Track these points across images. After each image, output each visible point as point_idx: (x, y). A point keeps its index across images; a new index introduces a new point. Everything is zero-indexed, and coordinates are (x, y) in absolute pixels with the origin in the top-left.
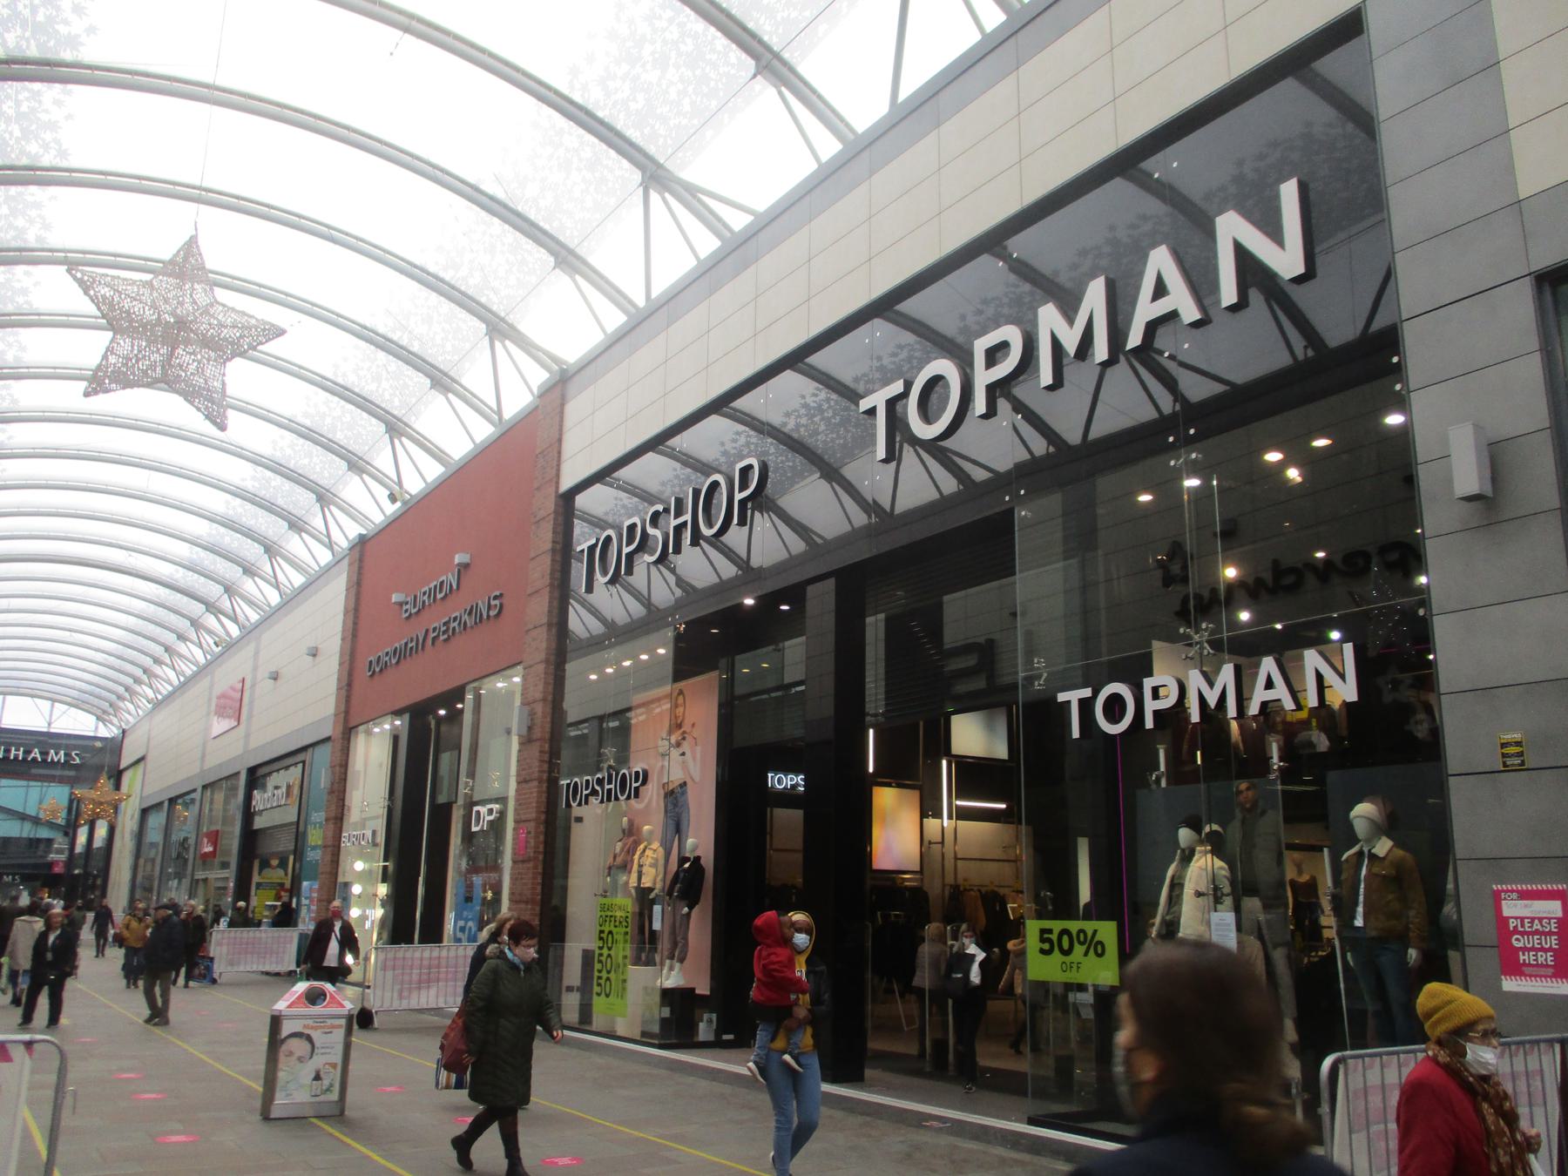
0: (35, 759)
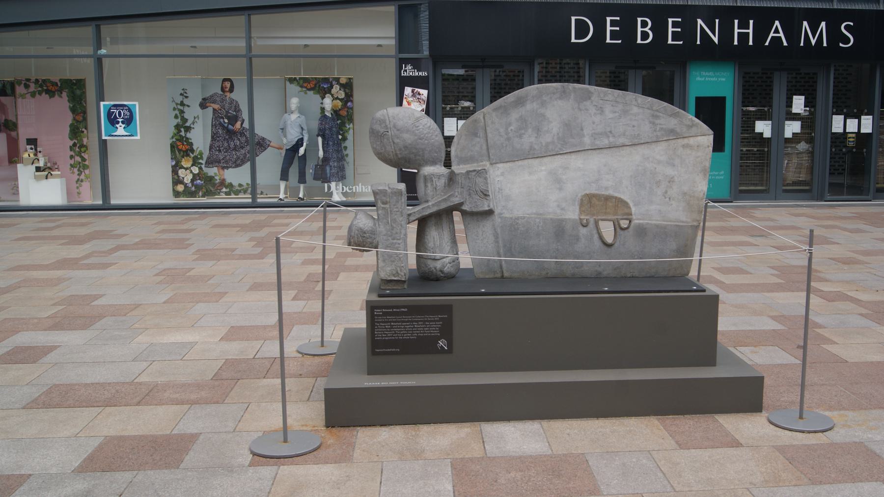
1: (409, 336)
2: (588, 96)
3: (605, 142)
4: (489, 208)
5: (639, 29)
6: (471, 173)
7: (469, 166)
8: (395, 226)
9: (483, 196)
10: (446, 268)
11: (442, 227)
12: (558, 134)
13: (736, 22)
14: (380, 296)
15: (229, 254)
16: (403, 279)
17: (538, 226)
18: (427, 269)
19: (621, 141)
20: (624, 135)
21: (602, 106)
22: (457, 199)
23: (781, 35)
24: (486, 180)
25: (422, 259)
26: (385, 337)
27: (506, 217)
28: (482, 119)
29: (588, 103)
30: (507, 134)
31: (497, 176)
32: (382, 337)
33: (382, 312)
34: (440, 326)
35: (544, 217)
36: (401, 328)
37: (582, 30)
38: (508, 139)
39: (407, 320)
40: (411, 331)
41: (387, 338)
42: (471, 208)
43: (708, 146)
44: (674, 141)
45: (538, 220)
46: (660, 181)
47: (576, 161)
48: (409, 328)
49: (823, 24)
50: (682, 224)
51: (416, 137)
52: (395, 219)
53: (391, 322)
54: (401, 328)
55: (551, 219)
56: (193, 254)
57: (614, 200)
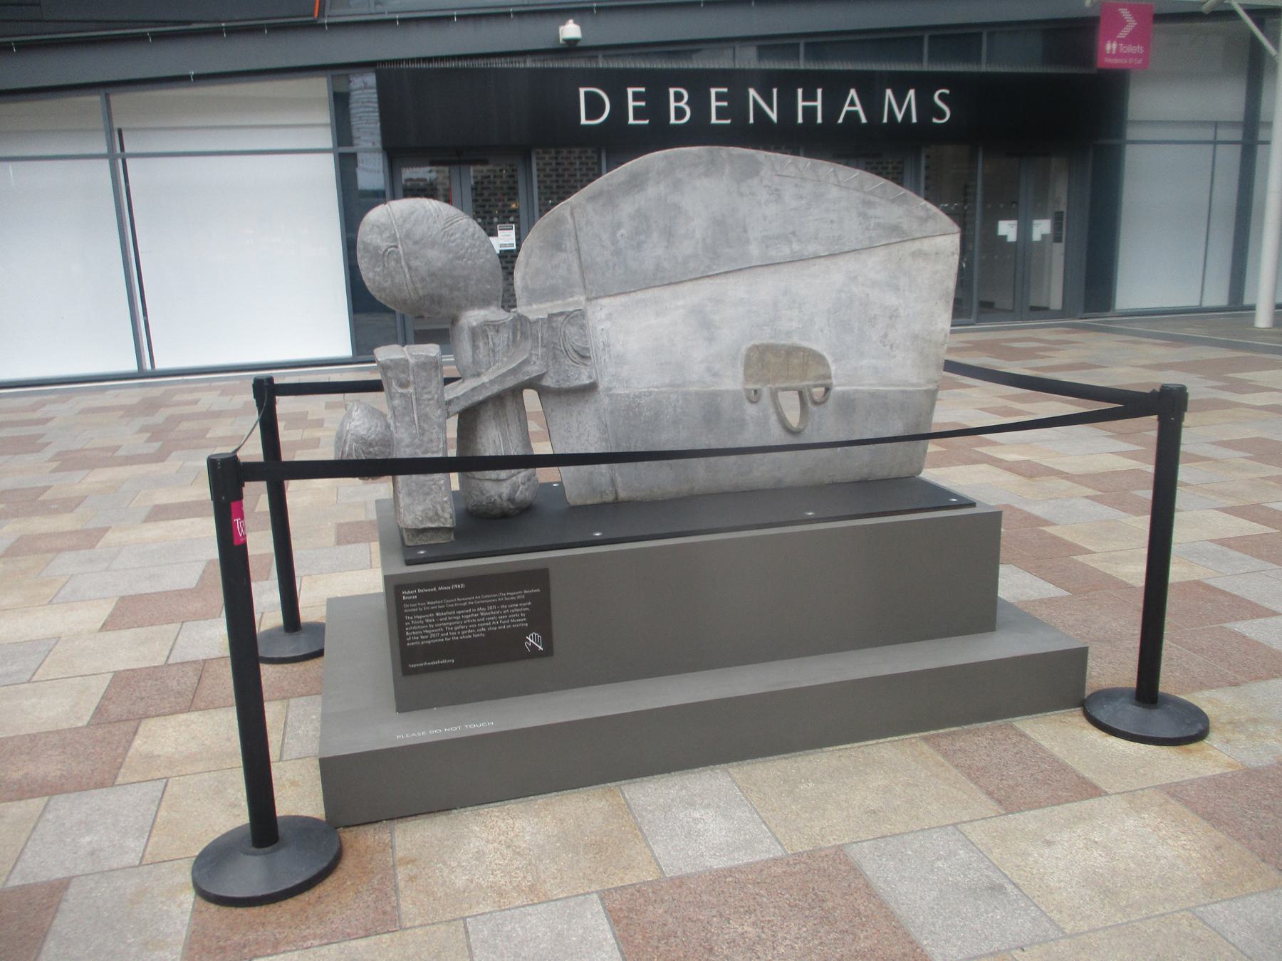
0: (852, 116)
1: (471, 634)
2: (753, 171)
3: (785, 251)
4: (591, 381)
5: (673, 105)
6: (555, 319)
7: (548, 304)
8: (426, 426)
9: (578, 359)
10: (518, 493)
11: (507, 421)
12: (704, 240)
13: (800, 91)
14: (409, 563)
15: (109, 457)
16: (448, 526)
17: (675, 407)
18: (484, 498)
19: (812, 248)
20: (816, 238)
21: (779, 188)
22: (536, 368)
23: (858, 108)
24: (584, 331)
25: (473, 481)
26: (425, 640)
27: (618, 395)
28: (569, 217)
29: (755, 181)
30: (614, 242)
31: (599, 321)
32: (420, 640)
33: (417, 594)
34: (527, 609)
35: (685, 389)
36: (455, 620)
37: (595, 106)
38: (617, 253)
39: (465, 604)
40: (473, 623)
41: (429, 642)
42: (558, 381)
43: (953, 254)
44: (897, 247)
45: (673, 397)
46: (875, 317)
47: (735, 288)
48: (470, 618)
49: (912, 93)
50: (911, 389)
51: (451, 256)
52: (426, 415)
53: (434, 611)
54: (455, 620)
55: (697, 393)
56: (50, 461)
57: (802, 353)
